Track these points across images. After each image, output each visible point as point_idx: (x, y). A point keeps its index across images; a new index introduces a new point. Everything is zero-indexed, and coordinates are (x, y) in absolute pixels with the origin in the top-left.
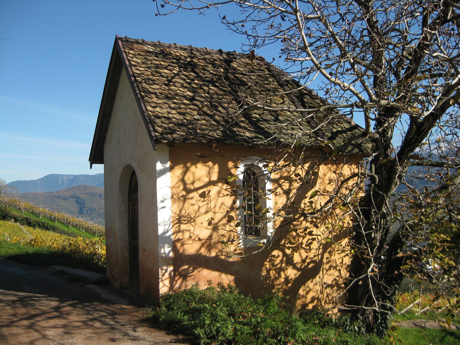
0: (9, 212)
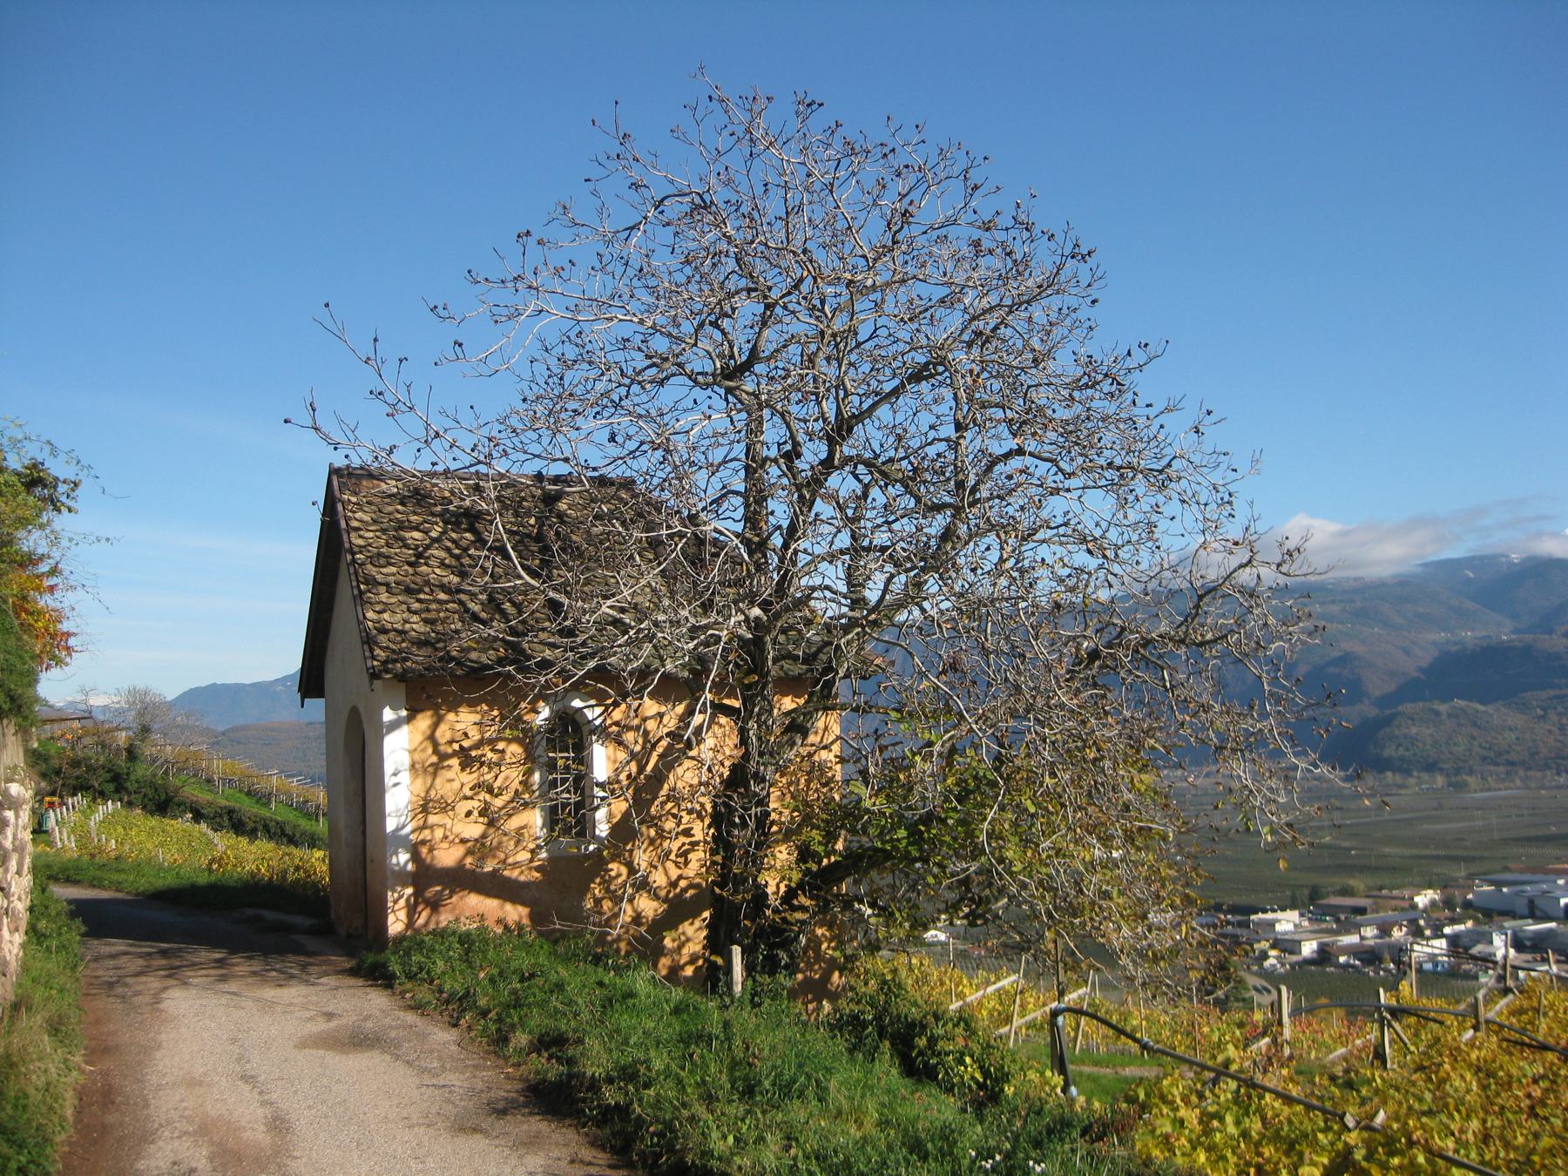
0: (177, 790)
